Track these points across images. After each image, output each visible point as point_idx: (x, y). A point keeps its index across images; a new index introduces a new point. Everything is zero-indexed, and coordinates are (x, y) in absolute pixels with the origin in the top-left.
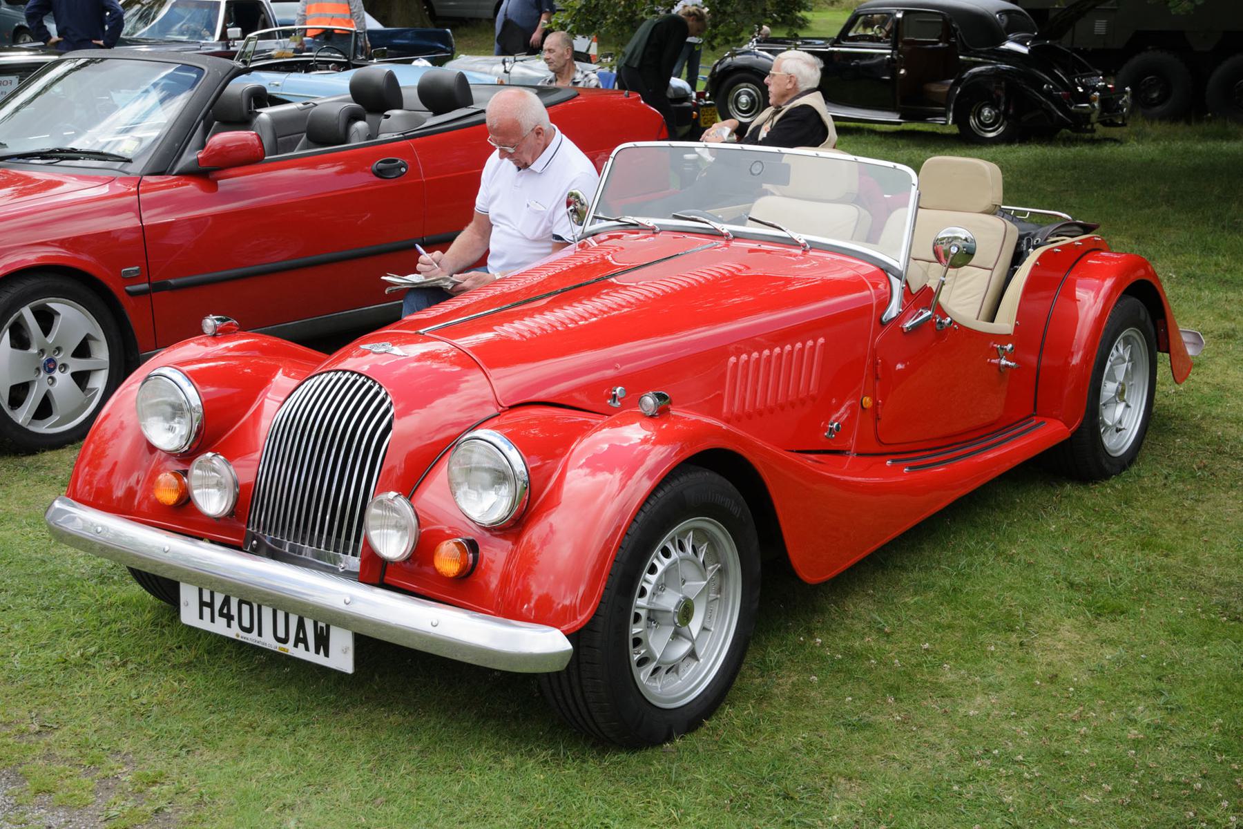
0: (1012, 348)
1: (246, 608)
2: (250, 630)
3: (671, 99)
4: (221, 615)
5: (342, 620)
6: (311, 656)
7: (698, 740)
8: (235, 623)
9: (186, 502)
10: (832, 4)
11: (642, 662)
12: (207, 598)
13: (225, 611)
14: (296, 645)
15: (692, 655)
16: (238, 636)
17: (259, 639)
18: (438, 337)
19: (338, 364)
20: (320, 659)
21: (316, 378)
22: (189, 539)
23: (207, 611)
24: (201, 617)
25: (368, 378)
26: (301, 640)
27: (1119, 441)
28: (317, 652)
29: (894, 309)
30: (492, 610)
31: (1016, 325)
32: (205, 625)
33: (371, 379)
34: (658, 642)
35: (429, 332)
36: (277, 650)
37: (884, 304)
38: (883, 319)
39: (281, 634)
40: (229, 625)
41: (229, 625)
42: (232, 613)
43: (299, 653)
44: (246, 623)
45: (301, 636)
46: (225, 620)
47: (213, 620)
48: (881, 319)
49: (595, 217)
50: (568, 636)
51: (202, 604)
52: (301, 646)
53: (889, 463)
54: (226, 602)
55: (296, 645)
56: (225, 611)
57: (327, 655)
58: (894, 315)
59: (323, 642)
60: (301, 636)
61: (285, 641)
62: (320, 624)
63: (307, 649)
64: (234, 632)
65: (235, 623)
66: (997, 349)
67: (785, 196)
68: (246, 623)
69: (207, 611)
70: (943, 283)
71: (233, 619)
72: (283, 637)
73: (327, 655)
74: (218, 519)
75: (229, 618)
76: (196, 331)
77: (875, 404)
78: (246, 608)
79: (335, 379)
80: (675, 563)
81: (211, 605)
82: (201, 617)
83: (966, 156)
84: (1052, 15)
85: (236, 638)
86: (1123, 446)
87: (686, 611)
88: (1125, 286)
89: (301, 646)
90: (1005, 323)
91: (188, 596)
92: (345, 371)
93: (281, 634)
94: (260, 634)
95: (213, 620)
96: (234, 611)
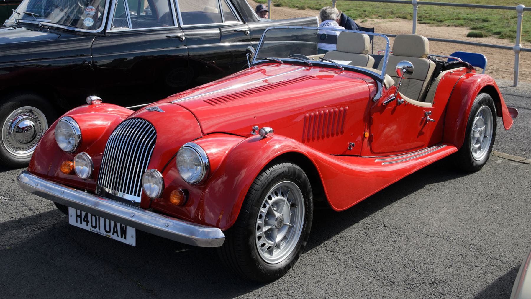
4: (84, 221)
13: (86, 219)
18: (28, 66)
23: (79, 219)
24: (77, 222)
32: (78, 225)
40: (87, 225)
41: (87, 225)
42: (89, 220)
46: (86, 223)
47: (81, 223)
56: (86, 219)
65: (90, 224)
69: (79, 219)
75: (87, 222)
81: (80, 216)
82: (77, 222)
95: (81, 223)
96: (89, 219)
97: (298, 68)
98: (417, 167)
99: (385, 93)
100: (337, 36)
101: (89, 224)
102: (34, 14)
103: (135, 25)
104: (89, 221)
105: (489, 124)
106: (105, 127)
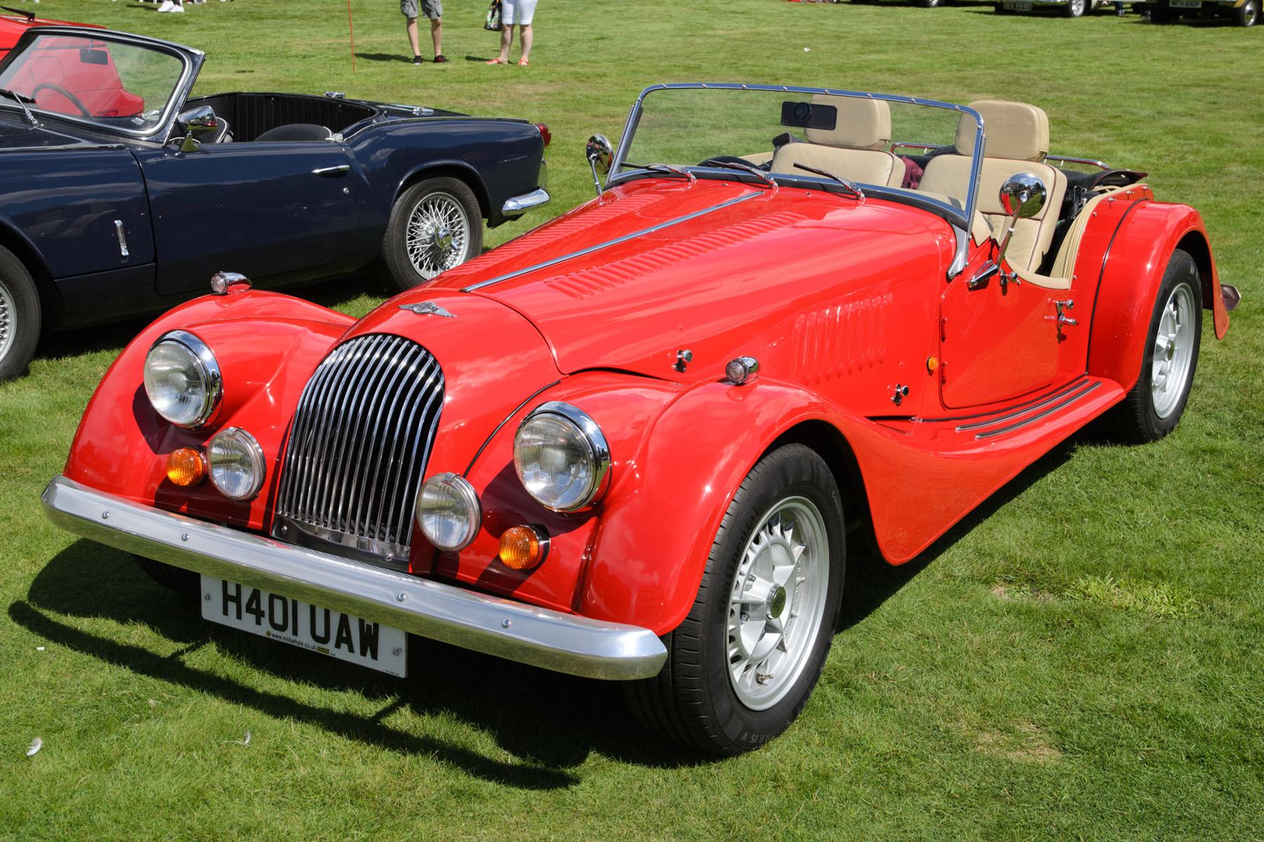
0: (1072, 304)
1: (278, 605)
2: (283, 628)
4: (249, 610)
5: (396, 616)
6: (356, 658)
8: (265, 621)
9: (203, 482)
10: (300, 2)
11: (736, 659)
12: (232, 591)
13: (254, 606)
14: (338, 646)
15: (781, 646)
16: (268, 633)
17: (293, 638)
19: (376, 325)
20: (367, 662)
21: (351, 343)
23: (232, 606)
24: (225, 612)
25: (404, 339)
26: (344, 639)
28: (363, 653)
29: (959, 263)
30: (565, 605)
31: (1074, 279)
33: (416, 343)
34: (749, 636)
35: (477, 290)
36: (316, 650)
37: (949, 258)
38: (950, 272)
39: (320, 632)
40: (258, 622)
41: (258, 622)
42: (262, 609)
43: (342, 654)
44: (279, 619)
45: (344, 635)
47: (239, 616)
48: (947, 273)
49: (622, 165)
50: (662, 638)
51: (227, 598)
52: (344, 647)
53: (957, 429)
54: (256, 595)
55: (338, 646)
56: (254, 606)
57: (375, 656)
58: (959, 270)
59: (370, 642)
60: (344, 635)
61: (325, 640)
62: (369, 622)
63: (351, 650)
64: (264, 630)
65: (265, 621)
66: (1056, 304)
67: (811, 142)
68: (279, 619)
69: (232, 606)
70: (1010, 234)
71: (264, 616)
73: (375, 656)
74: (240, 501)
75: (259, 614)
76: (205, 289)
77: (942, 365)
78: (278, 605)
79: (366, 342)
80: (766, 548)
81: (237, 599)
82: (225, 612)
85: (266, 635)
86: (1171, 404)
87: (777, 602)
88: (1177, 241)
89: (344, 647)
90: (1060, 280)
91: (211, 589)
92: (376, 335)
93: (320, 632)
94: (295, 632)
95: (239, 616)
96: (265, 606)
101: (262, 618)
104: (263, 612)
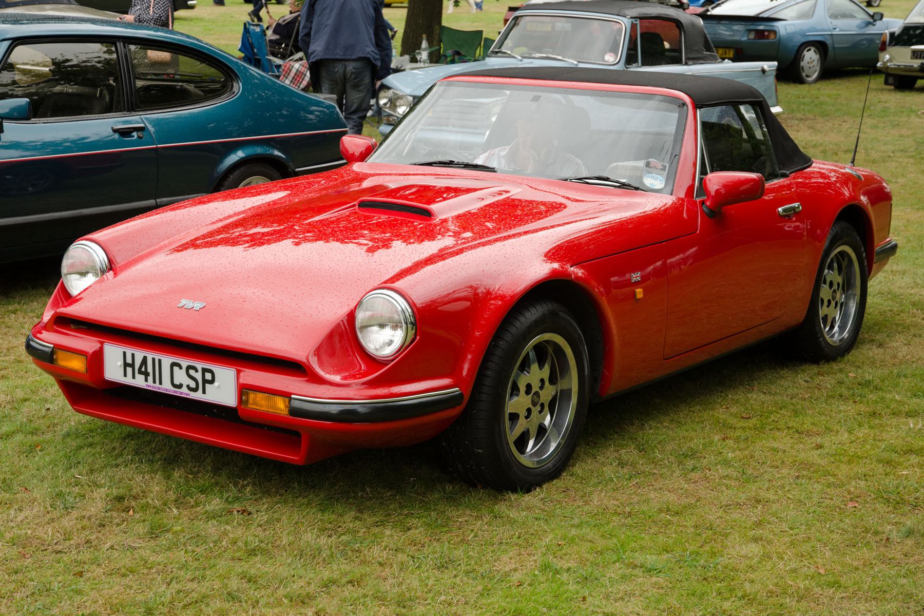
3: (392, 69)
4: (140, 372)
7: (565, 480)
8: (150, 378)
13: (143, 369)
18: (151, 202)
22: (701, 357)
23: (129, 370)
24: (125, 375)
27: (836, 335)
32: (128, 381)
40: (146, 380)
41: (146, 380)
42: (148, 371)
46: (143, 377)
47: (134, 377)
51: (126, 365)
56: (143, 369)
65: (150, 378)
69: (129, 370)
72: (127, 368)
75: (146, 374)
81: (132, 365)
82: (125, 375)
83: (107, 229)
84: (896, 34)
94: (161, 383)
95: (134, 377)
96: (150, 370)
97: (370, 39)
98: (618, 38)
99: (500, 48)
100: (429, 53)
102: (531, 443)
103: (537, 464)
104: (149, 373)
105: (531, 345)
106: (339, 323)
